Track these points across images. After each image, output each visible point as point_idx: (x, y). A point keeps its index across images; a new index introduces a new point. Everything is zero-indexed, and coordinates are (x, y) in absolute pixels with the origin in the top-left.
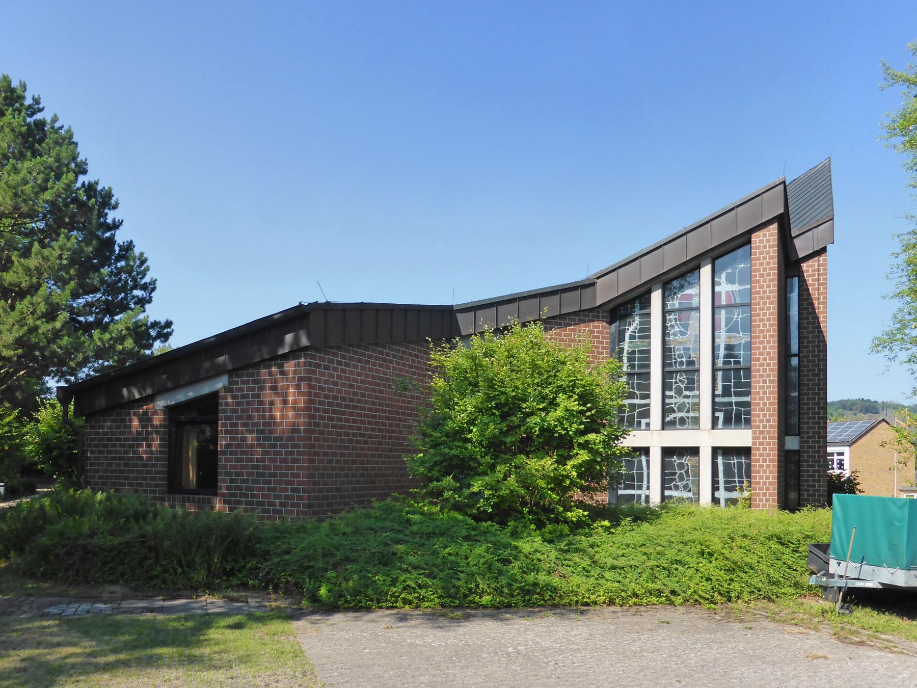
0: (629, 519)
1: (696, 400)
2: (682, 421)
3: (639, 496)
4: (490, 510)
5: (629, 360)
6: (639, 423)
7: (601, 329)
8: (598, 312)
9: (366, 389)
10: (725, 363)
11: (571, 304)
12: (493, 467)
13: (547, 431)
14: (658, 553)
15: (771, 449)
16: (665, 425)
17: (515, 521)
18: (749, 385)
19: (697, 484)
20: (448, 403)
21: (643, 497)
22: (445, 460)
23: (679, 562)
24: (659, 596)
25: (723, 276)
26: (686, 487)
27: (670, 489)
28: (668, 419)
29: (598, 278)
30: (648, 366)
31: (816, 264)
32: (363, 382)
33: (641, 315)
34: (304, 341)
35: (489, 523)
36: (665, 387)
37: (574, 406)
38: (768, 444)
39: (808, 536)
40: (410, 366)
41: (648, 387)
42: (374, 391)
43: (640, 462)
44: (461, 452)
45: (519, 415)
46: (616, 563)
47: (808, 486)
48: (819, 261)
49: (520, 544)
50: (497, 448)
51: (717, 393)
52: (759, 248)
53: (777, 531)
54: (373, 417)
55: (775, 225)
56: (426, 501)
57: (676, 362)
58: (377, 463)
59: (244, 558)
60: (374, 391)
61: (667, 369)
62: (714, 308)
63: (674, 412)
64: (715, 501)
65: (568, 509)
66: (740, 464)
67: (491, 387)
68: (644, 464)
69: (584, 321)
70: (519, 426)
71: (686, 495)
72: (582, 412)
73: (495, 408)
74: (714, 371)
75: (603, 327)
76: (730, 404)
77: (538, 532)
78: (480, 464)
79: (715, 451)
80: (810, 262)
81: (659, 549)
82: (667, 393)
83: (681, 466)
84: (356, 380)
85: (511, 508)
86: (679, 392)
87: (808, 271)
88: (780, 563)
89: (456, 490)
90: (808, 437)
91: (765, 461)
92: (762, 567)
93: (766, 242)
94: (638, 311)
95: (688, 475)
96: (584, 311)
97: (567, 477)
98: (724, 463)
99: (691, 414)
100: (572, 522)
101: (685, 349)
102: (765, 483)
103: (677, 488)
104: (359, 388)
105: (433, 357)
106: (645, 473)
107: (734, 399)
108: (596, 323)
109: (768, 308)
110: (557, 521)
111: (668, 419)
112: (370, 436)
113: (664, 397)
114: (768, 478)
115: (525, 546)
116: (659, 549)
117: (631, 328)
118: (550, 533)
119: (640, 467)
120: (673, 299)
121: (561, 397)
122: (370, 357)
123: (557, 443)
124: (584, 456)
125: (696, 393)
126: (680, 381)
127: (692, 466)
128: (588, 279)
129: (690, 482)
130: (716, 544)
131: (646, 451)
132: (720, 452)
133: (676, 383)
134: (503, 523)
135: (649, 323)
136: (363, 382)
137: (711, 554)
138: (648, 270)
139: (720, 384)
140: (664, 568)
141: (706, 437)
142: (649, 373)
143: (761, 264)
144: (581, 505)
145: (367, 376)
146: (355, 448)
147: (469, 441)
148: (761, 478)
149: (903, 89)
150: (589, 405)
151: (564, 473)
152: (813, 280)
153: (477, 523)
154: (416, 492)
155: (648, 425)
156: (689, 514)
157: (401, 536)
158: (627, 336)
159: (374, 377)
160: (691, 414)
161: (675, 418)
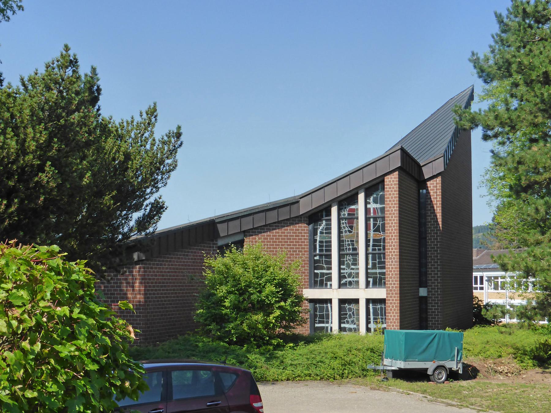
1: (357, 271)
2: (350, 283)
3: (327, 327)
4: (235, 340)
5: (320, 246)
6: (326, 285)
7: (303, 229)
9: (170, 276)
10: (373, 250)
11: (284, 214)
15: (396, 300)
16: (340, 286)
18: (384, 263)
19: (358, 320)
20: (213, 287)
22: (212, 316)
23: (321, 362)
24: (310, 376)
25: (372, 198)
26: (353, 322)
27: (344, 323)
28: (342, 282)
29: (300, 198)
30: (330, 251)
32: (169, 272)
33: (326, 220)
36: (340, 263)
37: (274, 289)
38: (395, 297)
40: (192, 259)
41: (330, 263)
42: (174, 276)
43: (327, 307)
46: (293, 363)
47: (432, 318)
48: (436, 181)
53: (371, 346)
54: (174, 290)
55: (397, 173)
57: (346, 249)
60: (174, 276)
61: (341, 253)
62: (367, 219)
64: (368, 330)
66: (381, 308)
71: (352, 326)
72: (278, 292)
75: (304, 227)
76: (376, 273)
79: (368, 301)
80: (432, 182)
81: (313, 356)
82: (342, 267)
83: (350, 309)
84: (165, 272)
87: (430, 187)
89: (218, 330)
90: (432, 289)
92: (360, 363)
93: (392, 182)
95: (354, 315)
96: (293, 218)
99: (355, 279)
100: (274, 345)
101: (351, 241)
102: (393, 319)
103: (348, 322)
105: (205, 261)
107: (378, 271)
109: (394, 220)
111: (342, 282)
113: (340, 269)
114: (394, 316)
117: (321, 228)
121: (268, 284)
122: (172, 258)
123: (264, 307)
124: (278, 313)
126: (349, 260)
129: (355, 319)
130: (340, 353)
131: (330, 301)
132: (371, 301)
137: (336, 358)
138: (330, 195)
140: (314, 365)
143: (390, 194)
145: (170, 269)
146: (166, 308)
148: (391, 316)
152: (433, 193)
155: (331, 285)
157: (194, 353)
159: (174, 269)
160: (355, 279)
161: (346, 281)
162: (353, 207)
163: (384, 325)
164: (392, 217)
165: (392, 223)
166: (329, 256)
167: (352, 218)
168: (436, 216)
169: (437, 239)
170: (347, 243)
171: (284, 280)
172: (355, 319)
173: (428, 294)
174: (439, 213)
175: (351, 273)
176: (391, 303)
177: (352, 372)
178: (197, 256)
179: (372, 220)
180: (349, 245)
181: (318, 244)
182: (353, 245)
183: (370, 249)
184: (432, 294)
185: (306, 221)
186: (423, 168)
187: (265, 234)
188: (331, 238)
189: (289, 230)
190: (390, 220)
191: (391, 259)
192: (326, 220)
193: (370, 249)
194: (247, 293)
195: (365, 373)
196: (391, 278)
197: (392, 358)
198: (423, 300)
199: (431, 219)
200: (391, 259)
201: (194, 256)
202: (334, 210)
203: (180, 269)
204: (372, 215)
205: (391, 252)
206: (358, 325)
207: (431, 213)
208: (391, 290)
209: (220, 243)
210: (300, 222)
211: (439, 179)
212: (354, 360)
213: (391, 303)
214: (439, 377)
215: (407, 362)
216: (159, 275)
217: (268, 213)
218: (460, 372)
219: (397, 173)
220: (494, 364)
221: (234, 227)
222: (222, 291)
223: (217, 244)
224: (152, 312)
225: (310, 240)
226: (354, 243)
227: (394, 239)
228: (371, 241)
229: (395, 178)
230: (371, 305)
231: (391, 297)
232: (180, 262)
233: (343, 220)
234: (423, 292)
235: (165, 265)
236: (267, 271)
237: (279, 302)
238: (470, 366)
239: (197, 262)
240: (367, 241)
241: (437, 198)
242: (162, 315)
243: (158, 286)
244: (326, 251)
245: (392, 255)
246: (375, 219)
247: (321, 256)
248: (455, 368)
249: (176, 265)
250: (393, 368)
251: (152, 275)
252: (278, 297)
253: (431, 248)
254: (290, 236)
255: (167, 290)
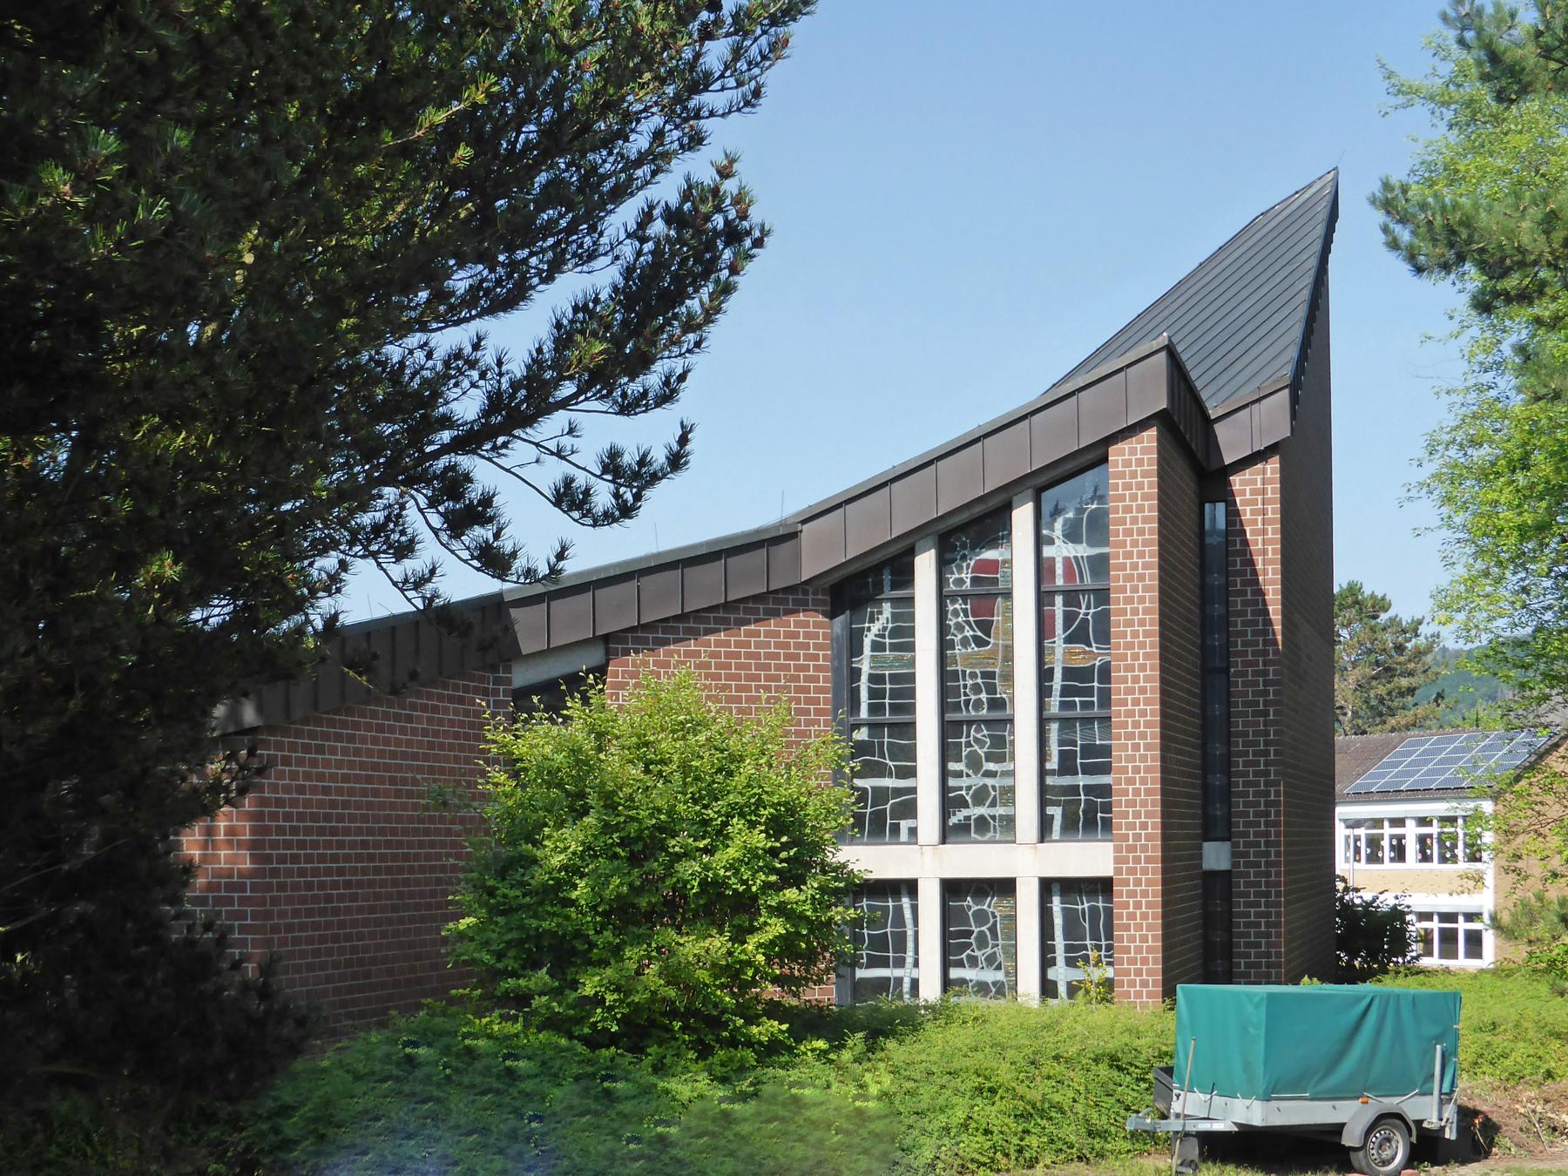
0: (861, 1035)
1: (1007, 782)
2: (982, 824)
3: (899, 981)
4: (615, 1028)
5: (873, 694)
6: (895, 830)
7: (812, 630)
8: (806, 593)
9: (351, 792)
10: (1063, 705)
11: (747, 579)
12: (617, 951)
13: (713, 887)
14: (908, 1092)
15: (1149, 883)
16: (948, 833)
17: (660, 1046)
18: (1106, 751)
19: (1012, 954)
21: (906, 986)
26: (991, 960)
27: (960, 964)
28: (953, 820)
29: (804, 522)
30: (911, 709)
31: (1259, 478)
32: (346, 778)
33: (895, 602)
34: (249, 715)
35: (613, 1049)
36: (947, 752)
37: (759, 839)
39: (1166, 1054)
40: (425, 733)
41: (910, 753)
42: (364, 792)
44: (559, 925)
45: (663, 857)
48: (1264, 472)
49: (673, 1084)
50: (627, 916)
51: (1048, 766)
52: (1122, 475)
53: (1111, 1046)
54: (365, 844)
55: (1152, 433)
56: (496, 1013)
57: (967, 702)
58: (372, 936)
59: (195, 1127)
61: (950, 716)
62: (1043, 598)
63: (965, 805)
64: (1048, 989)
65: (751, 1020)
66: (1094, 911)
67: (610, 804)
68: (908, 914)
69: (776, 613)
70: (662, 879)
71: (990, 976)
72: (773, 852)
73: (618, 845)
74: (1043, 722)
75: (816, 625)
76: (1074, 790)
77: (701, 1064)
78: (592, 945)
80: (1247, 474)
81: (909, 1085)
82: (952, 766)
83: (981, 917)
84: (333, 777)
85: (652, 1023)
86: (974, 763)
87: (1243, 493)
88: (1112, 1100)
89: (556, 993)
90: (1247, 845)
91: (1138, 905)
92: (1079, 1108)
93: (1136, 467)
94: (889, 593)
95: (995, 937)
96: (776, 592)
97: (749, 963)
98: (1063, 909)
99: (1000, 811)
100: (760, 1043)
101: (985, 675)
102: (1139, 950)
103: (973, 962)
104: (340, 791)
106: (910, 933)
107: (1082, 780)
108: (802, 617)
109: (1142, 600)
110: (733, 1043)
111: (953, 820)
112: (360, 884)
113: (944, 774)
115: (681, 1088)
116: (909, 1085)
117: (876, 628)
118: (723, 1065)
119: (899, 920)
120: (960, 570)
123: (727, 907)
125: (1007, 766)
126: (977, 740)
127: (1004, 918)
128: (782, 524)
129: (999, 951)
130: (1005, 1074)
132: (1056, 888)
133: (968, 744)
134: (638, 1049)
135: (912, 617)
136: (346, 778)
137: (993, 1091)
139: (1054, 749)
141: (1027, 859)
142: (914, 723)
143: (1128, 510)
144: (775, 1010)
145: (352, 765)
146: (336, 911)
147: (573, 903)
149: (1421, 111)
150: (784, 839)
151: (743, 957)
152: (1253, 512)
153: (593, 1051)
154: (463, 996)
155: (913, 832)
156: (976, 1019)
158: (867, 643)
159: (363, 766)
160: (1000, 811)
161: (968, 818)
162: (990, 554)
163: (1109, 972)
164: (1135, 589)
165: (1135, 612)
166: (909, 729)
167: (989, 595)
168: (1262, 593)
169: (1265, 673)
170: (970, 682)
171: (791, 808)
172: (999, 951)
173: (1235, 864)
174: (1273, 582)
175: (985, 786)
176: (1132, 894)
177: (1052, 1141)
178: (441, 722)
179: (1059, 600)
180: (976, 689)
181: (864, 685)
182: (991, 689)
183: (1054, 702)
184: (1248, 864)
185: (822, 603)
186: (1218, 428)
187: (712, 638)
188: (912, 663)
189: (765, 635)
190: (1129, 601)
191: (1130, 736)
192: (893, 601)
193: (1054, 702)
194: (663, 857)
195: (1098, 1143)
196: (1132, 804)
197: (1212, 1089)
198: (1217, 885)
199: (1244, 603)
200: (1130, 736)
201: (430, 721)
202: (925, 564)
203: (387, 767)
204: (1060, 582)
205: (1130, 714)
206: (1014, 972)
207: (1244, 583)
208: (1131, 849)
209: (521, 676)
210: (801, 606)
211: (1272, 467)
212: (1057, 1098)
213: (1132, 894)
214: (1384, 1155)
215: (1274, 1104)
216: (314, 790)
217: (691, 572)
218: (1450, 1134)
219: (1152, 433)
220: (1547, 1101)
221: (572, 620)
222: (561, 846)
223: (509, 681)
224: (290, 928)
225: (836, 671)
226: (995, 681)
227: (1143, 668)
228: (1058, 675)
229: (1145, 451)
230: (1056, 900)
231: (1132, 871)
232: (387, 742)
233: (954, 602)
234: (1216, 856)
235: (333, 751)
236: (730, 774)
237: (777, 888)
238: (1476, 1113)
239: (441, 746)
240: (1044, 675)
241: (1264, 532)
242: (322, 939)
243: (308, 831)
244: (895, 709)
245: (1136, 725)
246: (1071, 597)
247: (874, 727)
248: (1432, 1122)
249: (370, 753)
250: (1218, 1127)
251: (287, 789)
252: (774, 871)
253: (1246, 704)
254: (768, 656)
255: (341, 845)
